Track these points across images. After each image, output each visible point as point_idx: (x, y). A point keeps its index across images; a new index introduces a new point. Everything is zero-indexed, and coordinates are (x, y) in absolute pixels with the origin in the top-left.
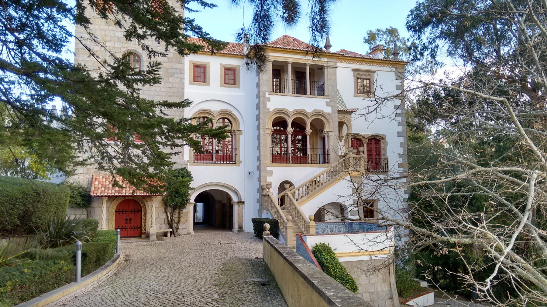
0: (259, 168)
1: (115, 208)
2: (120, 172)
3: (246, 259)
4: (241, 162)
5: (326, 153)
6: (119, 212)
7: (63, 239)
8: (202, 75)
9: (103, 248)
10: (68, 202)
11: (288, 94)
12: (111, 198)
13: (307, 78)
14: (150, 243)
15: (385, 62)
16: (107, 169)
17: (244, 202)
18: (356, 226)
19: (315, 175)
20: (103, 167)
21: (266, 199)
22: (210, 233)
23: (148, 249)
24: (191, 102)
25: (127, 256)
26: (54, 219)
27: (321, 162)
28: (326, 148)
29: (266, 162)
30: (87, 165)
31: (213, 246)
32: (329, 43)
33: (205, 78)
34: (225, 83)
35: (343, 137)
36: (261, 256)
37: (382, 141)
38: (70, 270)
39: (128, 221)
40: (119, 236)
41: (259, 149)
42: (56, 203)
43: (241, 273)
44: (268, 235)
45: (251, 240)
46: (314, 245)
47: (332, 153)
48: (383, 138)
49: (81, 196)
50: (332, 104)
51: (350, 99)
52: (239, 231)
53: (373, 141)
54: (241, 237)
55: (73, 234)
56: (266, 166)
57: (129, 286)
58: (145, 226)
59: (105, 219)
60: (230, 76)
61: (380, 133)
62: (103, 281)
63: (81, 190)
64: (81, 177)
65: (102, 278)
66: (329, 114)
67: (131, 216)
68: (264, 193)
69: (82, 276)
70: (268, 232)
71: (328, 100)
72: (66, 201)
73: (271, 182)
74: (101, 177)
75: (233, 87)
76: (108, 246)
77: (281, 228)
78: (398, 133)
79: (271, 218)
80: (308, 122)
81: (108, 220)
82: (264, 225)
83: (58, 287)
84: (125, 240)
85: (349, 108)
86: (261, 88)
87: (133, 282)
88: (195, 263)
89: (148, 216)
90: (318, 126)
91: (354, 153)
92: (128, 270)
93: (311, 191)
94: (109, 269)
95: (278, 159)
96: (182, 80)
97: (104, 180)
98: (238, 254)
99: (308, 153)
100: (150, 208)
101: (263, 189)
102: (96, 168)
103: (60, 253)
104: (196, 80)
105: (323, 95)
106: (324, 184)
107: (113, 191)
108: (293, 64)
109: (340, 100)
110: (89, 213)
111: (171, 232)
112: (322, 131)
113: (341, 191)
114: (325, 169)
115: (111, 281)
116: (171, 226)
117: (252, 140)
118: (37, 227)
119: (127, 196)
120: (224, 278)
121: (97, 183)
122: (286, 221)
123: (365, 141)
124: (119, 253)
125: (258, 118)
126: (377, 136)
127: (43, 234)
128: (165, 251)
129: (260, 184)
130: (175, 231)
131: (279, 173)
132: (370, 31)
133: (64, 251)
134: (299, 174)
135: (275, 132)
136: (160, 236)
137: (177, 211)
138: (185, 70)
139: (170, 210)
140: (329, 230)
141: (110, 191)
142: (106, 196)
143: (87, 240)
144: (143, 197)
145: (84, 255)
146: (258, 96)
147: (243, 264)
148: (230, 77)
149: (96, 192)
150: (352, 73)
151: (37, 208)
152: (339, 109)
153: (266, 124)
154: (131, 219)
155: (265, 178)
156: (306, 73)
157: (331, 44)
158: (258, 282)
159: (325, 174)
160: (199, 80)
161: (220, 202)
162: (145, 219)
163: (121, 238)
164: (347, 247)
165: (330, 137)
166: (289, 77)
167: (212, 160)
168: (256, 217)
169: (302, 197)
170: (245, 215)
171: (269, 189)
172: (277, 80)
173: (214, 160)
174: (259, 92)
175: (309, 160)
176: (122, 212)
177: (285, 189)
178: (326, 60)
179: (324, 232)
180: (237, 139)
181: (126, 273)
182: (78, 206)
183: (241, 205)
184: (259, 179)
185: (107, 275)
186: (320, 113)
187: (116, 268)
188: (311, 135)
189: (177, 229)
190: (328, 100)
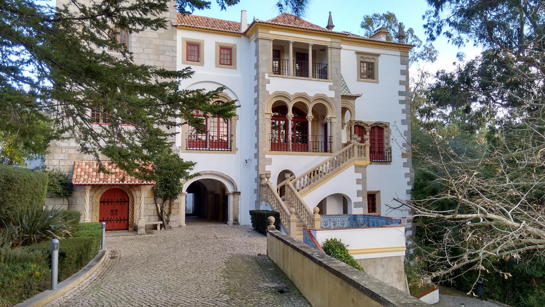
0: (257, 156)
1: (99, 198)
2: (107, 151)
3: (249, 257)
4: (237, 149)
5: (329, 140)
6: (104, 202)
7: (38, 234)
8: (196, 54)
9: (85, 246)
10: (46, 190)
11: (289, 77)
12: (95, 187)
13: (308, 59)
14: (138, 237)
15: (388, 45)
16: (91, 152)
17: (240, 193)
18: (361, 220)
19: (317, 164)
20: (86, 149)
21: (265, 189)
22: (204, 226)
23: (136, 244)
24: (193, 72)
25: (113, 252)
26: (28, 211)
27: (320, 151)
28: (329, 135)
29: (264, 149)
30: (63, 138)
31: (209, 241)
32: (332, 23)
33: (198, 57)
34: (221, 64)
35: (345, 124)
36: (264, 252)
37: (385, 129)
38: (44, 275)
39: (114, 212)
40: (104, 229)
41: (257, 135)
42: (32, 191)
43: (250, 275)
44: (273, 229)
45: (249, 234)
46: (324, 241)
47: (334, 140)
48: (386, 126)
49: (61, 184)
50: (335, 88)
51: (354, 85)
52: (234, 224)
53: (376, 129)
54: (238, 230)
55: (50, 228)
56: (264, 153)
57: (119, 294)
58: (133, 218)
59: (88, 210)
60: (225, 56)
61: (383, 120)
62: (85, 286)
63: (61, 178)
64: (62, 163)
65: (84, 283)
66: (331, 98)
67: (117, 206)
68: (263, 182)
69: (59, 281)
70: (273, 226)
71: (332, 84)
72: (43, 189)
73: (270, 171)
74: (84, 164)
75: (230, 68)
76: (92, 242)
77: (282, 221)
78: (402, 120)
79: (271, 210)
80: (310, 107)
81: (92, 211)
82: (269, 218)
83: (28, 297)
84: (111, 233)
85: (353, 93)
86: (260, 69)
87: (123, 287)
88: (193, 262)
89: (136, 207)
90: (320, 111)
91: (357, 141)
92: (115, 272)
93: (314, 182)
94: (93, 269)
95: (276, 147)
96: (174, 58)
97: (87, 167)
98: (238, 251)
99: (310, 140)
100: (139, 199)
101: (261, 179)
102: (78, 150)
103: (31, 253)
104: (189, 59)
105: (326, 78)
106: (327, 174)
107: (98, 180)
108: (295, 43)
109: (343, 85)
110: (70, 203)
111: (161, 225)
112: (324, 118)
113: (346, 182)
114: (327, 158)
115: (96, 285)
116: (161, 219)
117: (249, 126)
118: (8, 220)
119: (113, 185)
120: (232, 282)
121: (79, 170)
122: (289, 213)
123: (368, 129)
124: (104, 249)
125: (257, 101)
126: (380, 124)
127: (16, 229)
128: (156, 246)
129: (258, 173)
130: (165, 223)
131: (277, 162)
132: (367, 16)
133: (37, 250)
134: (300, 163)
135: (274, 118)
136: (149, 229)
137: (168, 201)
138: (177, 48)
139: (160, 200)
140: (332, 223)
141: (94, 180)
142: (89, 185)
143: (67, 235)
144: (131, 186)
145: (62, 255)
146: (257, 78)
147: (248, 262)
148: (226, 57)
149: (78, 180)
150: (355, 56)
151: (8, 197)
152: (342, 94)
153: (266, 108)
154: (117, 211)
155: (264, 167)
156: (308, 55)
157: (334, 24)
158: (275, 288)
159: (328, 163)
160: (193, 59)
161: (212, 192)
162: (133, 211)
163: (106, 230)
164: (361, 242)
165: (333, 124)
166: (290, 58)
167: (206, 147)
168: (253, 209)
169: (303, 188)
170: (242, 207)
171: (268, 178)
172: (277, 62)
173: (208, 146)
174: (258, 73)
175: (311, 148)
176: (108, 202)
177: (285, 179)
178: (330, 40)
179: (326, 225)
180: (233, 124)
181: (113, 275)
182: (58, 195)
183: (237, 196)
184: (257, 168)
185: (90, 277)
186: (323, 98)
187: (101, 267)
188: (313, 121)
189: (168, 221)
190: (332, 84)
